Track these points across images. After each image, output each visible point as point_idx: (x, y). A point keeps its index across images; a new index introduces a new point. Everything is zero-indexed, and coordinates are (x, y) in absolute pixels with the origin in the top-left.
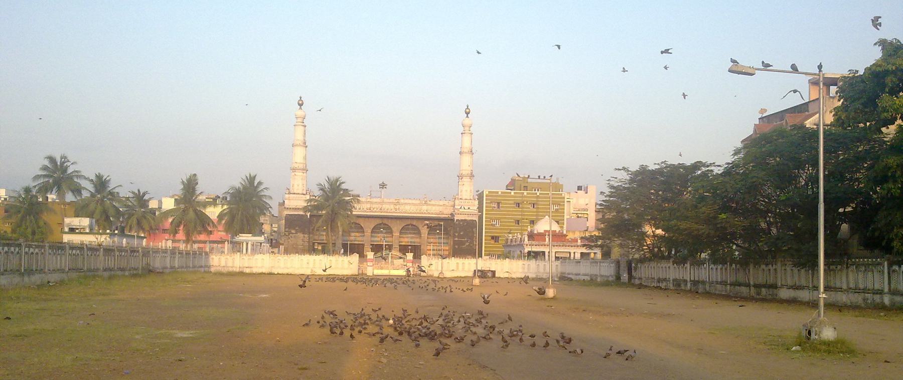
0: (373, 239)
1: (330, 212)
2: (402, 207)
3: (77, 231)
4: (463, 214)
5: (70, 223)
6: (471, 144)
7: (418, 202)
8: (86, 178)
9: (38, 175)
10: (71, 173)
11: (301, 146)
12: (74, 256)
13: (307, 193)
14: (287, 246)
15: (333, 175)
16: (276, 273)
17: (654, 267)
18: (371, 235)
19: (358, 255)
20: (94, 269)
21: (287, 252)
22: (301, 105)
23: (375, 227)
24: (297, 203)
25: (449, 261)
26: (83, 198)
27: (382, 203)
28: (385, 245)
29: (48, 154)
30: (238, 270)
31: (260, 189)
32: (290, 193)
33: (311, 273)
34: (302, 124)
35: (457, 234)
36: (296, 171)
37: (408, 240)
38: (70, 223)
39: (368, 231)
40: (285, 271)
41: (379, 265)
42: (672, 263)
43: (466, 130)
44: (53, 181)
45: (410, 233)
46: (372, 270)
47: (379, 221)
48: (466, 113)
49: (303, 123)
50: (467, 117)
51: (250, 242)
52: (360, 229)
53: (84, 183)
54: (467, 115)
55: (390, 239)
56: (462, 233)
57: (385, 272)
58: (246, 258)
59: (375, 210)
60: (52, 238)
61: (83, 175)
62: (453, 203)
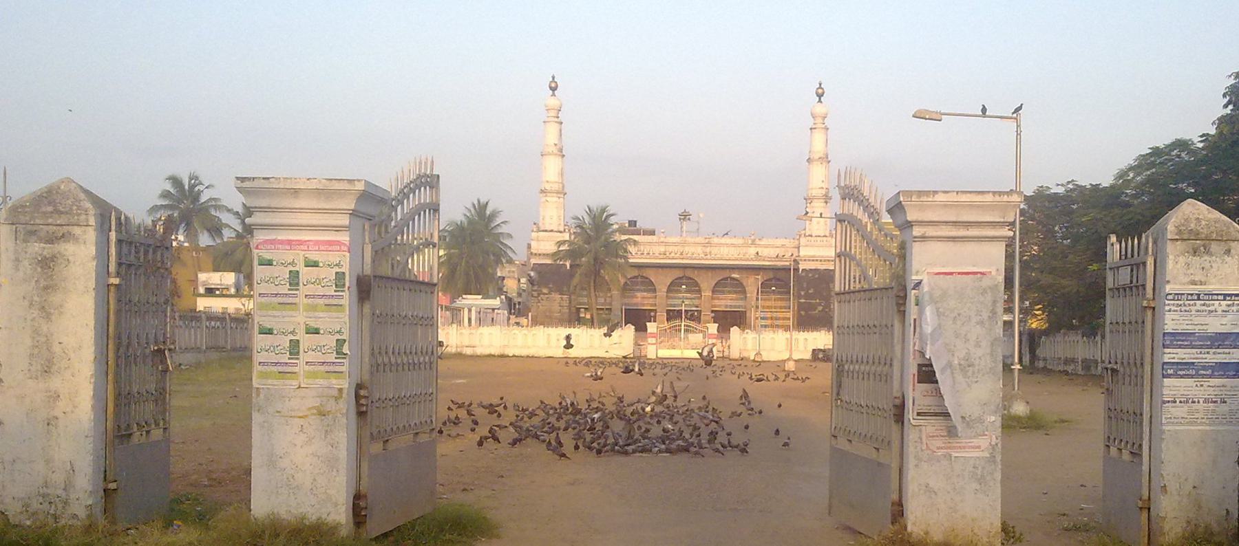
0: (671, 302)
1: (592, 262)
2: (715, 250)
3: (217, 292)
4: (813, 260)
5: (207, 281)
6: (826, 146)
7: (740, 241)
8: (229, 210)
9: (156, 206)
10: (205, 202)
11: (556, 154)
12: (213, 330)
13: (565, 230)
14: (535, 314)
15: (596, 205)
16: (511, 355)
17: (1078, 342)
18: (667, 296)
19: (633, 327)
20: (240, 348)
21: (536, 322)
22: (553, 89)
23: (672, 282)
24: (546, 245)
25: (773, 336)
26: (225, 240)
27: (684, 243)
28: (685, 311)
29: (169, 174)
30: (454, 350)
31: (496, 224)
32: (539, 231)
33: (563, 354)
34: (556, 120)
35: (803, 293)
36: (548, 194)
37: (727, 302)
38: (207, 281)
39: (662, 290)
40: (524, 352)
41: (670, 343)
42: (1080, 336)
43: (819, 123)
44: (179, 214)
45: (730, 292)
46: (655, 350)
47: (678, 273)
48: (817, 96)
49: (558, 117)
50: (820, 101)
51: (473, 309)
52: (650, 287)
53: (226, 218)
54: (820, 99)
55: (696, 302)
56: (810, 292)
57: (676, 353)
58: (466, 331)
59: (673, 255)
60: (183, 304)
61: (224, 206)
62: (797, 242)
